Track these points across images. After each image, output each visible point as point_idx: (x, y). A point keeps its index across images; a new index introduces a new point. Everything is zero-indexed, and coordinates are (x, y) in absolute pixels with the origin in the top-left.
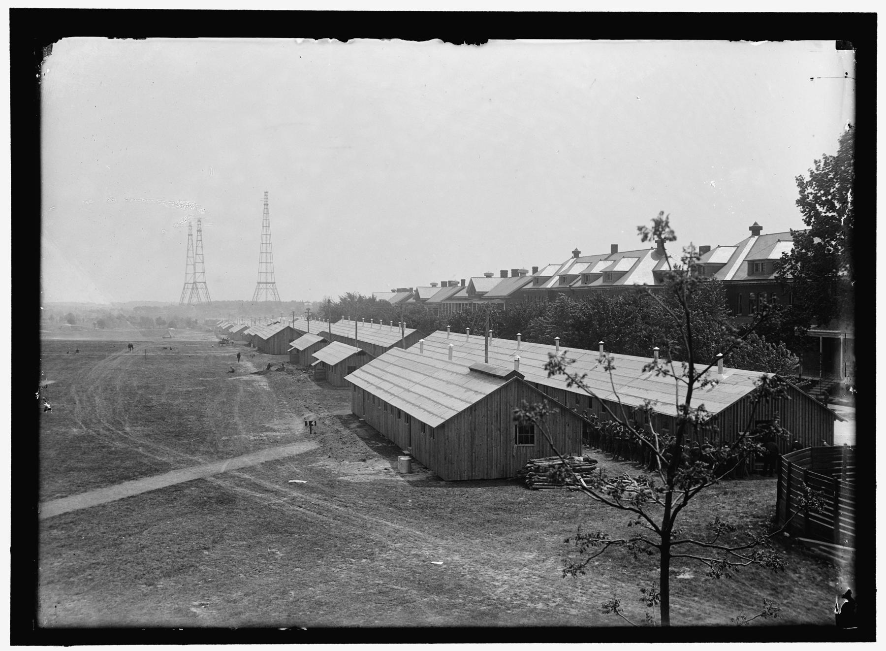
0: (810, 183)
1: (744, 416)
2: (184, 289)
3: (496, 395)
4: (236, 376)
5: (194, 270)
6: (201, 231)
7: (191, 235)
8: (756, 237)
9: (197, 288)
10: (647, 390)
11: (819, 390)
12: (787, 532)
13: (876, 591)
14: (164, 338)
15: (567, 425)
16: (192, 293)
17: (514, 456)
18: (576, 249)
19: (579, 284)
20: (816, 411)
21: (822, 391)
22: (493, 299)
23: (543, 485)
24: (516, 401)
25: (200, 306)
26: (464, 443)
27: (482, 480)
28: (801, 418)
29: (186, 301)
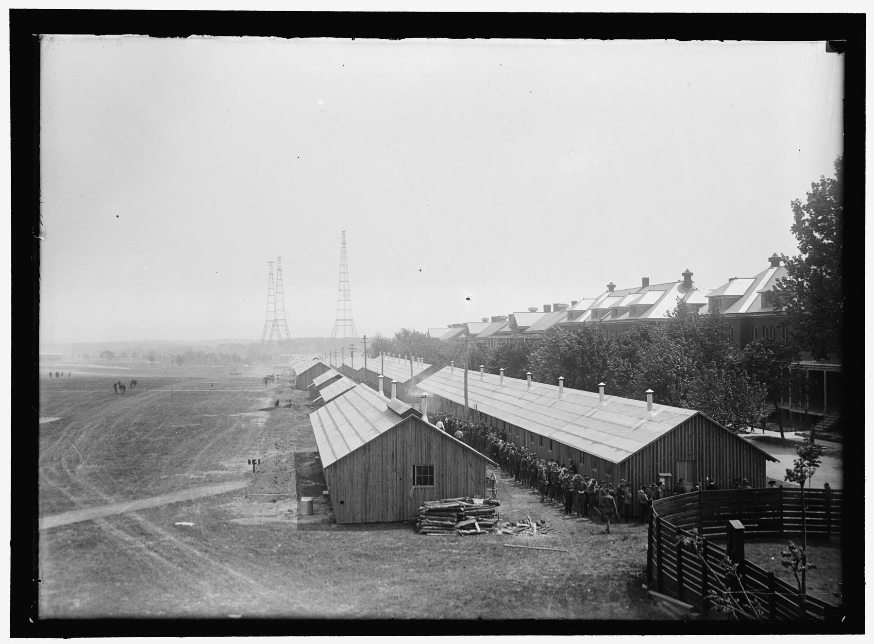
0: (807, 208)
1: (664, 456)
2: (265, 326)
3: (392, 434)
6: (281, 270)
7: (271, 274)
8: (775, 268)
9: (278, 326)
10: (586, 428)
11: (822, 427)
12: (645, 584)
13: (865, 584)
14: (231, 374)
15: (469, 465)
16: (272, 330)
17: (410, 498)
18: (611, 283)
19: (609, 318)
20: (745, 451)
21: (825, 427)
22: (531, 334)
23: (433, 529)
24: (413, 439)
25: (281, 343)
26: (357, 485)
27: (378, 523)
28: (728, 458)
29: (267, 338)
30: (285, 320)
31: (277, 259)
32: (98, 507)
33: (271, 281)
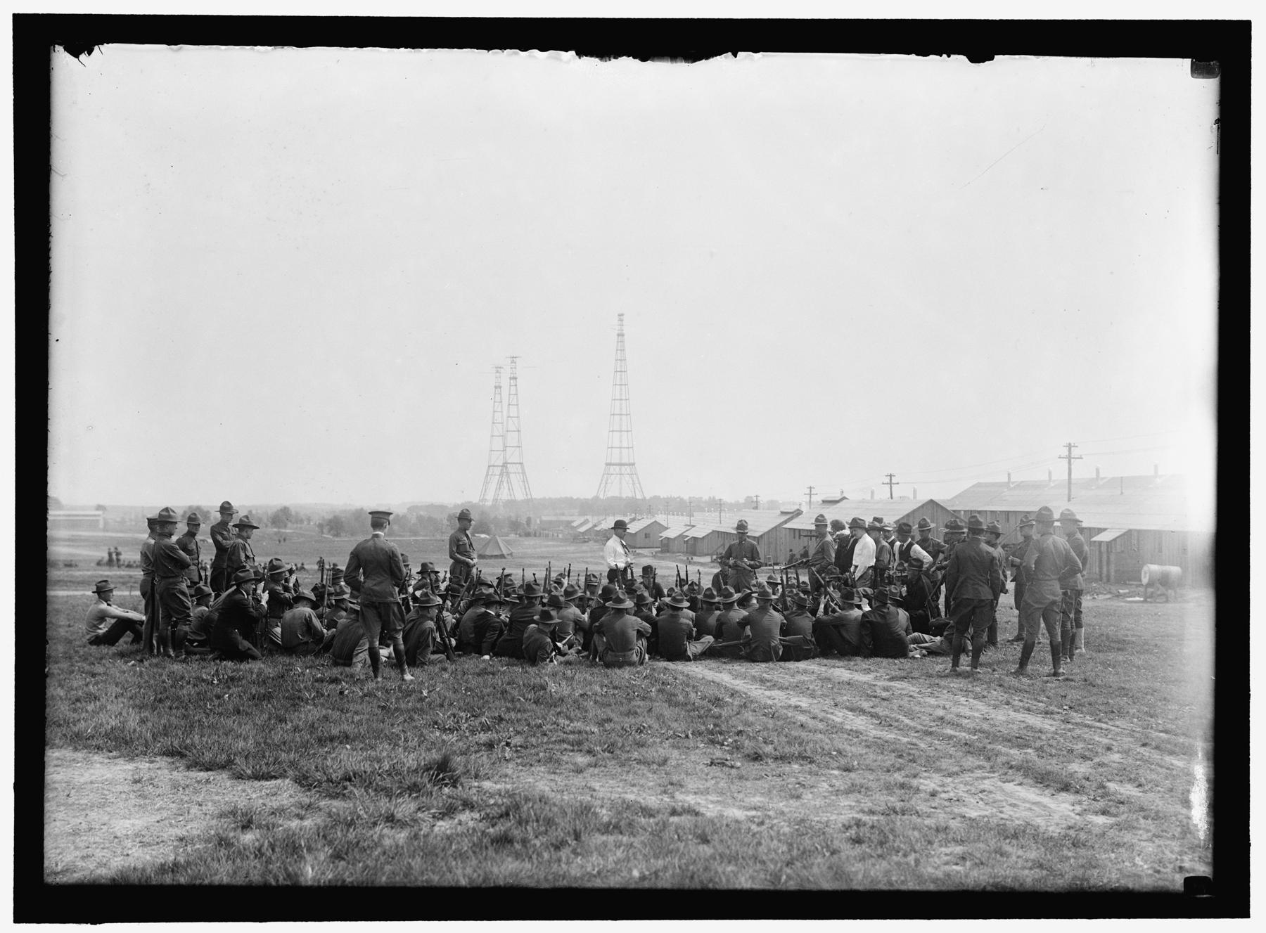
2: (487, 475)
4: (79, 570)
5: (504, 444)
6: (500, 387)
9: (508, 474)
30: (521, 464)
31: (509, 360)
32: (220, 771)
33: (513, 392)
